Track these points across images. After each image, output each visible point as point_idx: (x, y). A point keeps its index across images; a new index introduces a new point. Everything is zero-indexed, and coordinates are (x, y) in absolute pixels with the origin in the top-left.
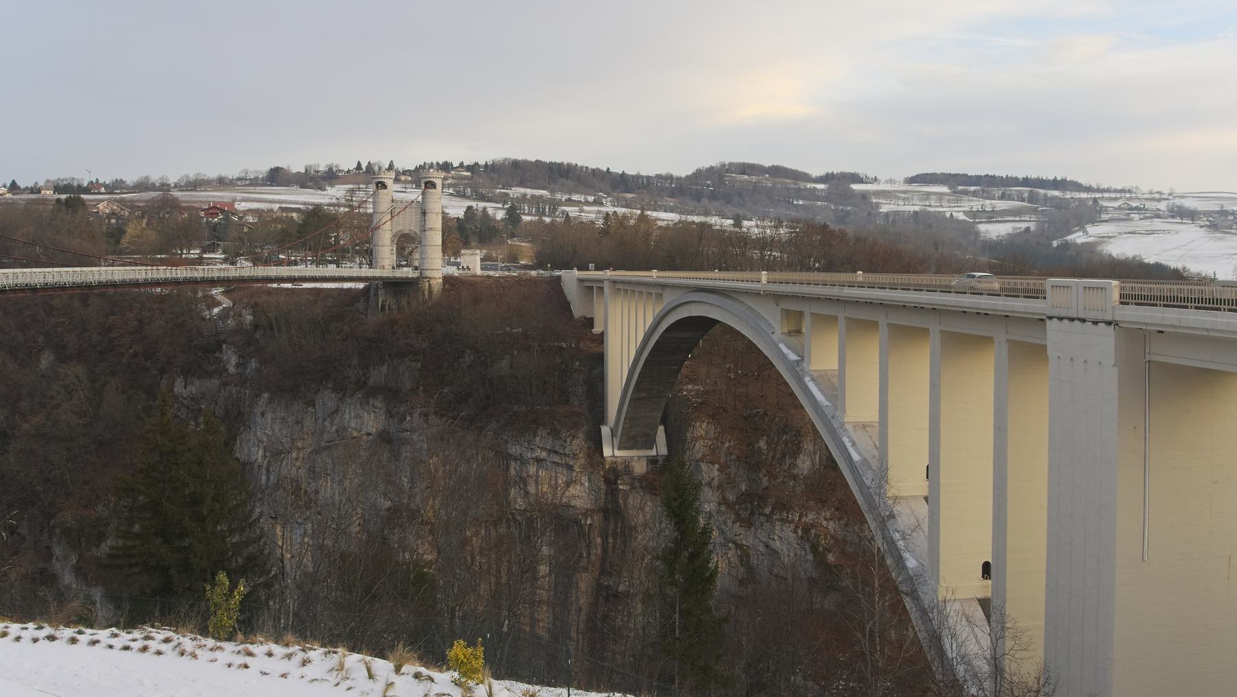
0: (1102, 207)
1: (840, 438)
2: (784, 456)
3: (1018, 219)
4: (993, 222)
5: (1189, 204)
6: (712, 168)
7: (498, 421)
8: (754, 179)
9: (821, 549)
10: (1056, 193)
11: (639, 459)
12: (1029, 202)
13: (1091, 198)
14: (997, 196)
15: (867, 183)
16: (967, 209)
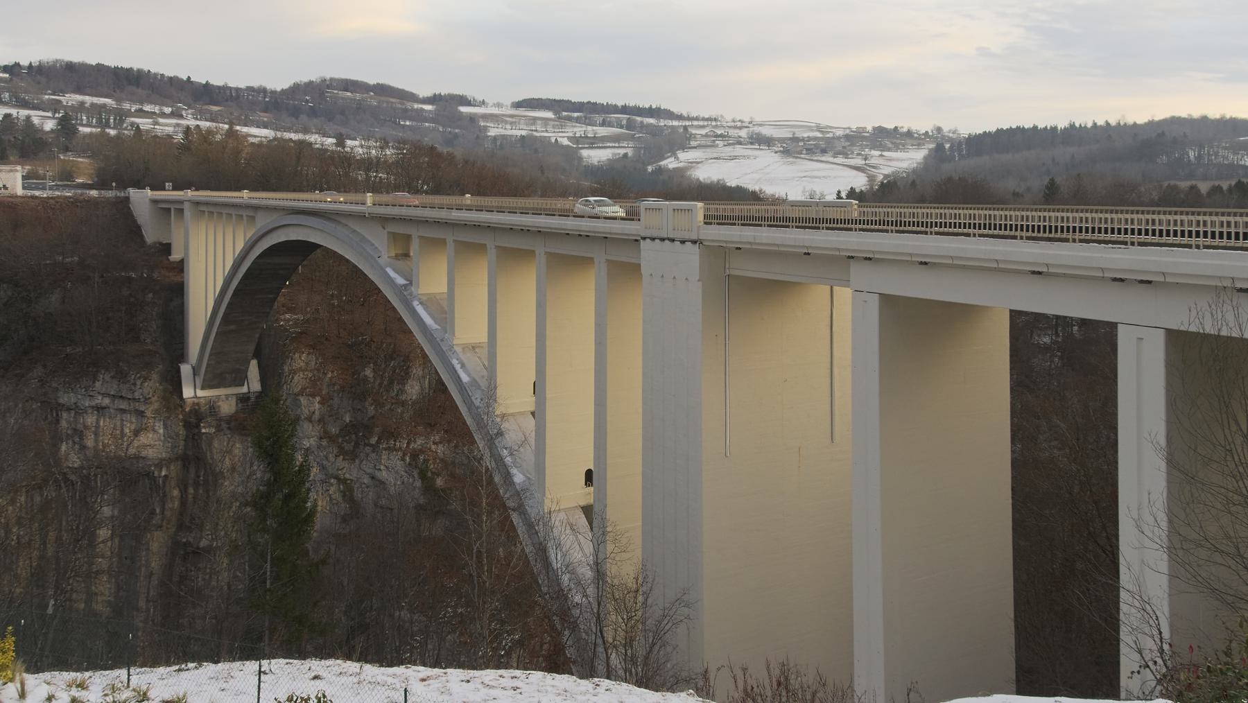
0: (691, 134)
2: (391, 382)
3: (617, 145)
5: (767, 131)
6: (311, 83)
7: (45, 366)
8: (358, 96)
9: (429, 474)
10: (652, 121)
12: (627, 129)
13: (681, 126)
14: (598, 122)
15: (475, 106)
16: (571, 135)
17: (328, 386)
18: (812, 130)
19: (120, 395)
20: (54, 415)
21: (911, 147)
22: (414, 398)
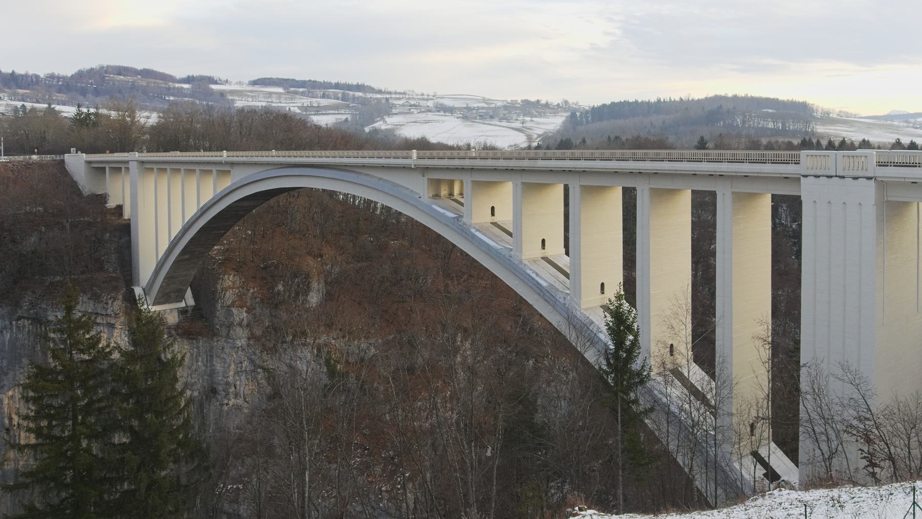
0: (393, 104)
1: (524, 271)
2: (297, 294)
3: (336, 112)
4: (320, 114)
5: (448, 103)
6: (92, 69)
7: (34, 292)
8: (130, 79)
9: (332, 362)
10: (360, 94)
11: (171, 312)
12: (342, 100)
13: (383, 98)
14: (319, 95)
15: (221, 84)
16: (300, 105)
17: (251, 299)
18: (480, 102)
19: (96, 312)
20: (43, 329)
21: (549, 115)
22: (314, 306)
